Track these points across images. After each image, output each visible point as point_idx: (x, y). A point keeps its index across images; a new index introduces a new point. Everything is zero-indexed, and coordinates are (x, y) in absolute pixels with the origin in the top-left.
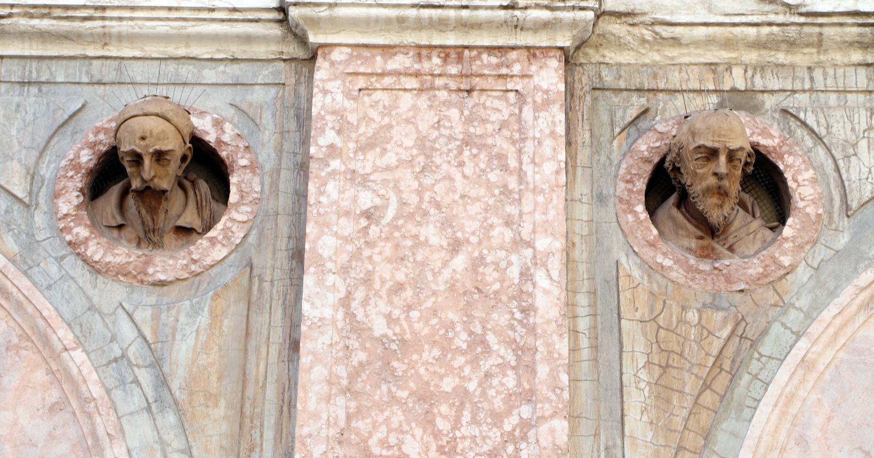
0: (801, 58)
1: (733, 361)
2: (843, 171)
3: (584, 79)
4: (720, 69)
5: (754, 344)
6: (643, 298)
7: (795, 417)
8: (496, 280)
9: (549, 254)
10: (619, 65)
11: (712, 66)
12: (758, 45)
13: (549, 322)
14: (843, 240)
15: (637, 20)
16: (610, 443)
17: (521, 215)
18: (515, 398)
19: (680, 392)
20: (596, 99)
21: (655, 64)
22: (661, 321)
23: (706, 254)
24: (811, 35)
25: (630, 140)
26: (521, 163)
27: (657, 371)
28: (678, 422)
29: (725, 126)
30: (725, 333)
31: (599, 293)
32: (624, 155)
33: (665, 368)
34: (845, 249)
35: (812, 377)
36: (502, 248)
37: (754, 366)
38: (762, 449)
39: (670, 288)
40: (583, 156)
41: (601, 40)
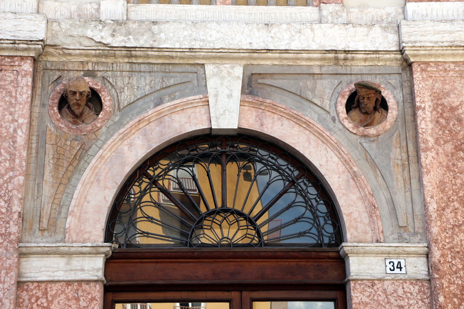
0: (110, 60)
1: (80, 157)
2: (119, 97)
3: (41, 66)
4: (85, 63)
5: (87, 151)
6: (54, 137)
7: (97, 173)
8: (5, 132)
9: (22, 124)
10: (53, 61)
11: (82, 62)
12: (95, 56)
13: (21, 146)
14: (117, 118)
15: (57, 47)
16: (39, 182)
17: (15, 111)
18: (7, 170)
19: (62, 166)
20: (44, 73)
21: (64, 61)
22: (58, 144)
23: (75, 123)
24: (112, 53)
25: (55, 86)
26: (16, 94)
27: (56, 160)
28: (60, 176)
29: (78, 84)
30: (78, 148)
31: (40, 136)
32: (52, 91)
33: (58, 159)
34: (117, 121)
35: (103, 161)
36: (8, 122)
37: (86, 158)
38: (85, 183)
39: (63, 134)
40: (39, 91)
41: (46, 53)
